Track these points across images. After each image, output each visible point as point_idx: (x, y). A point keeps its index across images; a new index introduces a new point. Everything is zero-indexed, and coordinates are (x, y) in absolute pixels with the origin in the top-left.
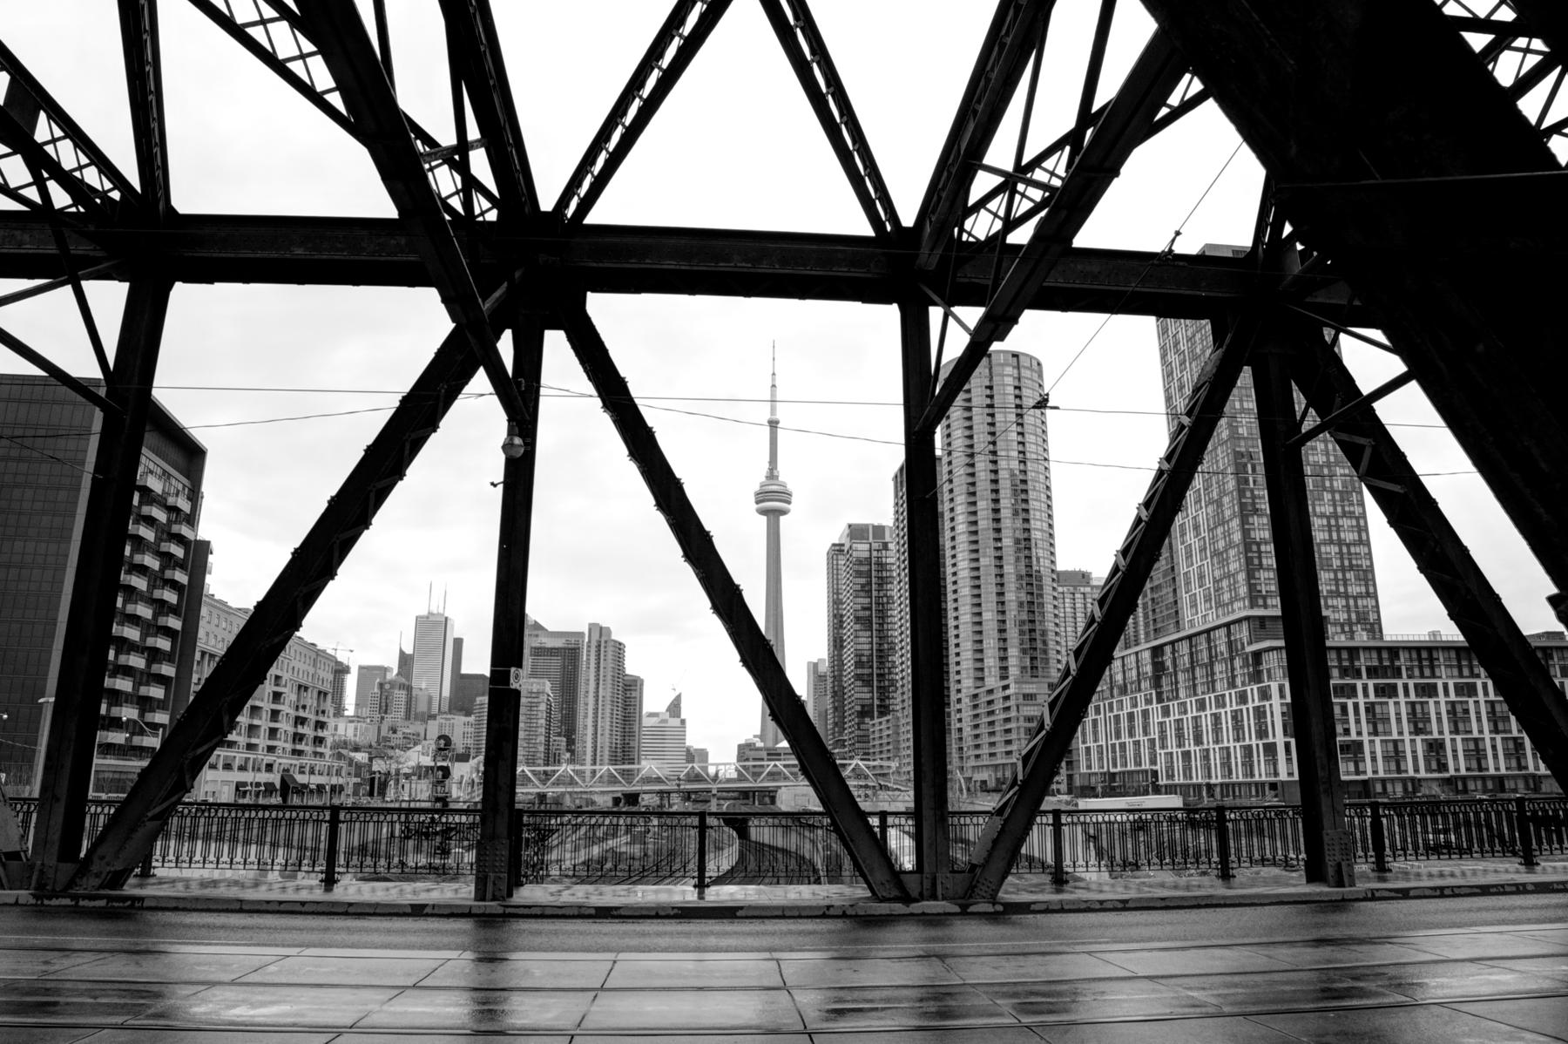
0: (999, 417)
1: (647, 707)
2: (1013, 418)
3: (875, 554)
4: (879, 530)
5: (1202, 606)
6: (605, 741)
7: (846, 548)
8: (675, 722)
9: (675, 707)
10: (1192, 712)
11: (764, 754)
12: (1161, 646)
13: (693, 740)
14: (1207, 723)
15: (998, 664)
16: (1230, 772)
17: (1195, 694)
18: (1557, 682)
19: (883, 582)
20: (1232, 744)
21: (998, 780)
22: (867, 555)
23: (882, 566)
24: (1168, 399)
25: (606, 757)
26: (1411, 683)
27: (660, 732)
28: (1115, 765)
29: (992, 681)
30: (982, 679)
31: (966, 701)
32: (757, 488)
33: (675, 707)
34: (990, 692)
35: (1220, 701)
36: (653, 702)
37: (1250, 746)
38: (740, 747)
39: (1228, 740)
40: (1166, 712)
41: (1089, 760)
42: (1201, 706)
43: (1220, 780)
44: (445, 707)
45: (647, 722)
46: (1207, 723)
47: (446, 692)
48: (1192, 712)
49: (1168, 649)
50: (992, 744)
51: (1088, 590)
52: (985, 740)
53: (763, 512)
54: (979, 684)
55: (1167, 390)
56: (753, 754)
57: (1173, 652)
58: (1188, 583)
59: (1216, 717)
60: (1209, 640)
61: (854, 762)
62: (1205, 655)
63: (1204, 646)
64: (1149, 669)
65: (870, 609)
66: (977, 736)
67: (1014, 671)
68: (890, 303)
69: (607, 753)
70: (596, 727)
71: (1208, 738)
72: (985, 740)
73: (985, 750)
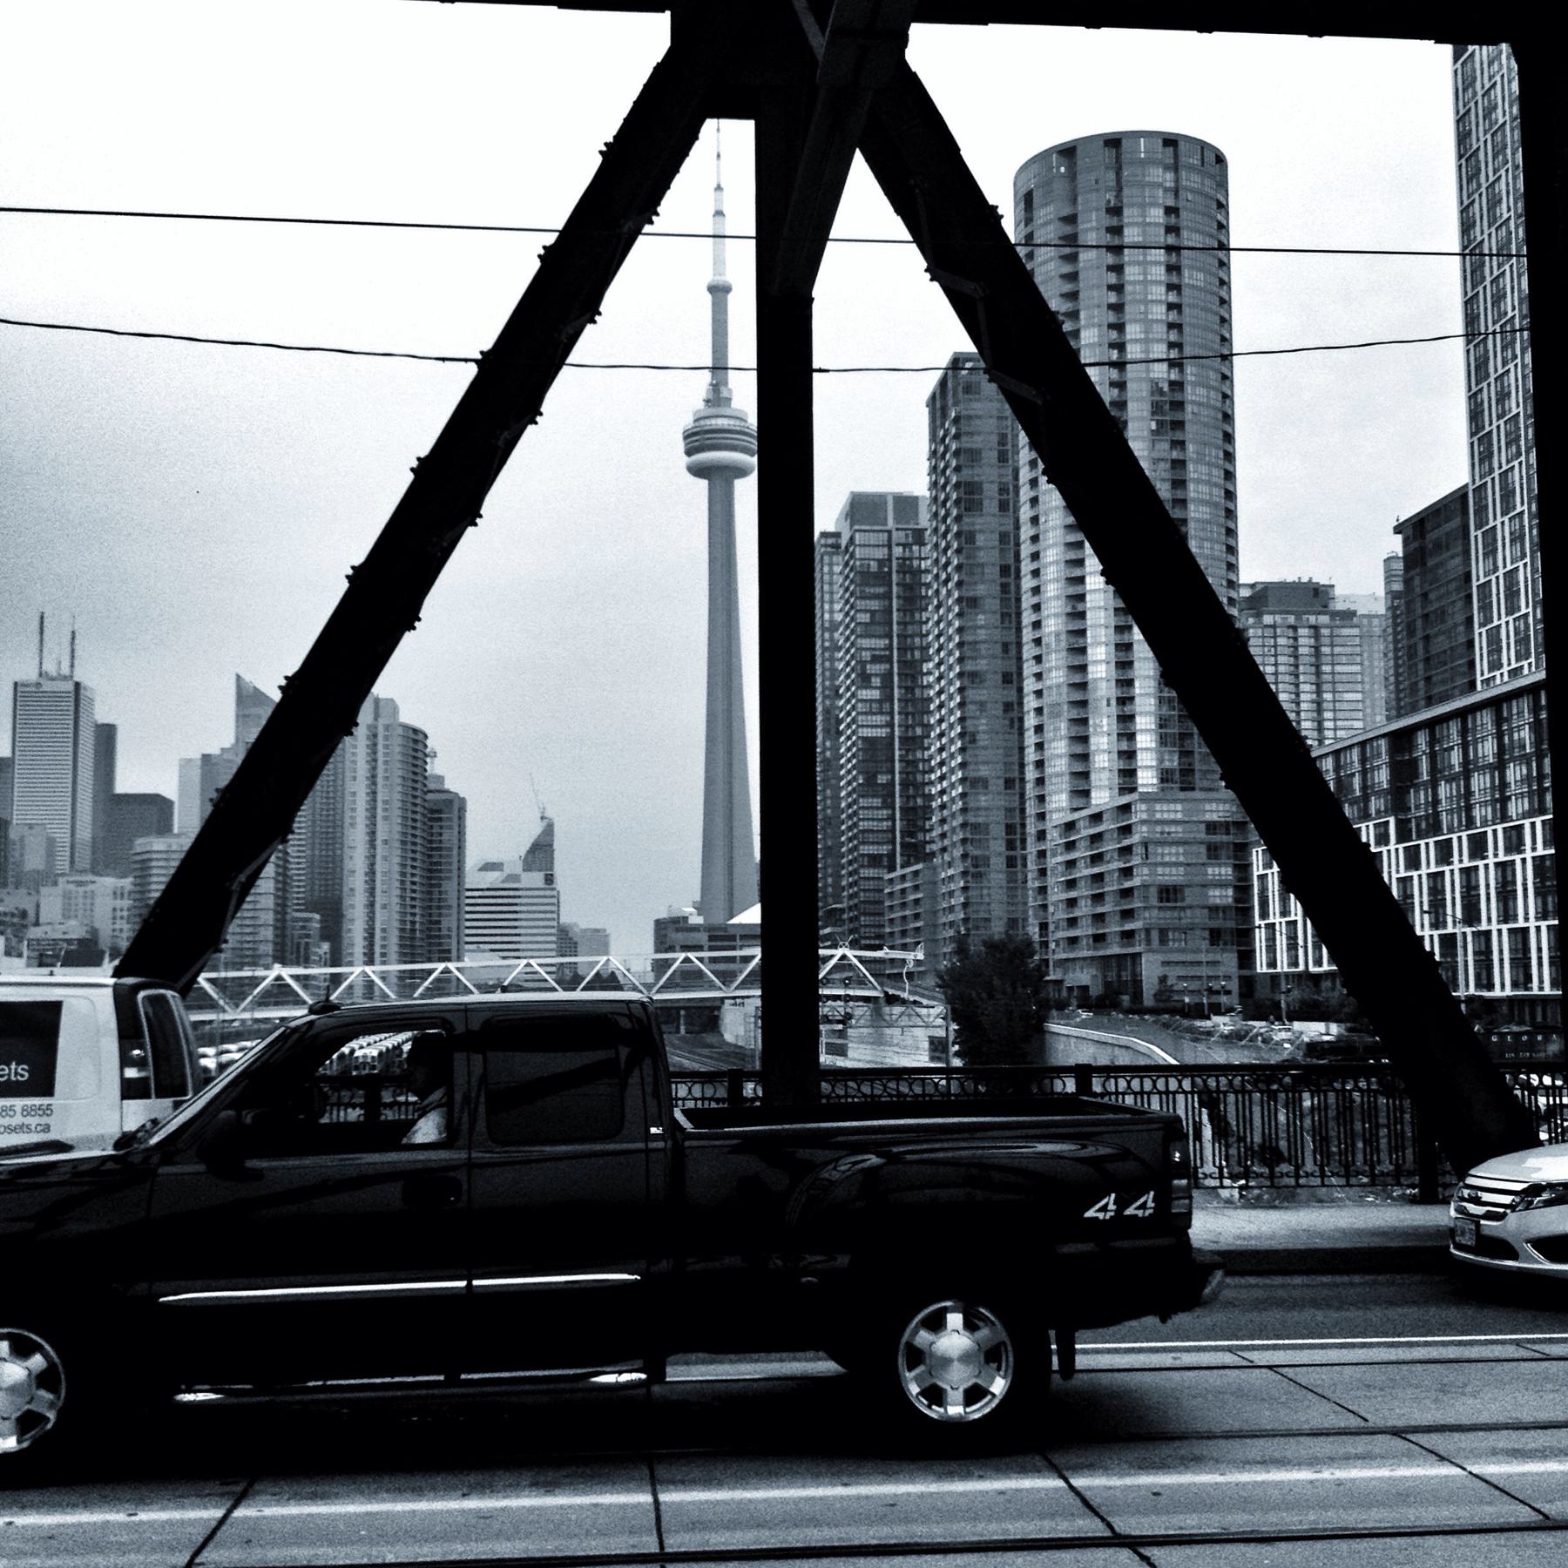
0: (1132, 273)
1: (475, 854)
2: (1159, 273)
3: (898, 551)
4: (906, 504)
5: (1508, 656)
6: (388, 919)
7: (844, 541)
8: (535, 879)
9: (541, 852)
10: (1462, 859)
11: (703, 938)
12: (1411, 731)
13: (576, 913)
14: (1487, 882)
15: (1118, 764)
16: (1529, 978)
17: (1505, 817)
18: (1276, 869)
19: (913, 600)
20: (1494, 927)
21: (1107, 985)
22: (881, 553)
23: (911, 574)
24: (1466, 226)
25: (394, 948)
26: (1464, 835)
27: (504, 898)
28: (1319, 963)
29: (1102, 797)
30: (1086, 794)
31: (1055, 838)
32: (687, 421)
33: (541, 852)
34: (1097, 818)
35: (1478, 847)
36: (490, 841)
37: (1525, 931)
38: (658, 922)
39: (1490, 918)
40: (1413, 860)
41: (1271, 948)
42: (1478, 847)
43: (1508, 992)
44: (84, 859)
45: (474, 878)
46: (1487, 882)
47: (85, 833)
48: (1462, 859)
49: (1422, 739)
50: (1099, 918)
51: (1324, 619)
52: (1084, 909)
53: (698, 471)
54: (1079, 802)
55: (1464, 210)
56: (679, 937)
57: (1432, 742)
58: (1486, 607)
59: (1469, 873)
60: (1499, 721)
61: (839, 952)
62: (1456, 758)
63: (1455, 738)
64: (1382, 777)
65: (889, 660)
66: (1072, 903)
67: (1147, 779)
68: (690, 137)
69: (394, 940)
70: (371, 891)
71: (1489, 907)
72: (1084, 909)
73: (1084, 930)
